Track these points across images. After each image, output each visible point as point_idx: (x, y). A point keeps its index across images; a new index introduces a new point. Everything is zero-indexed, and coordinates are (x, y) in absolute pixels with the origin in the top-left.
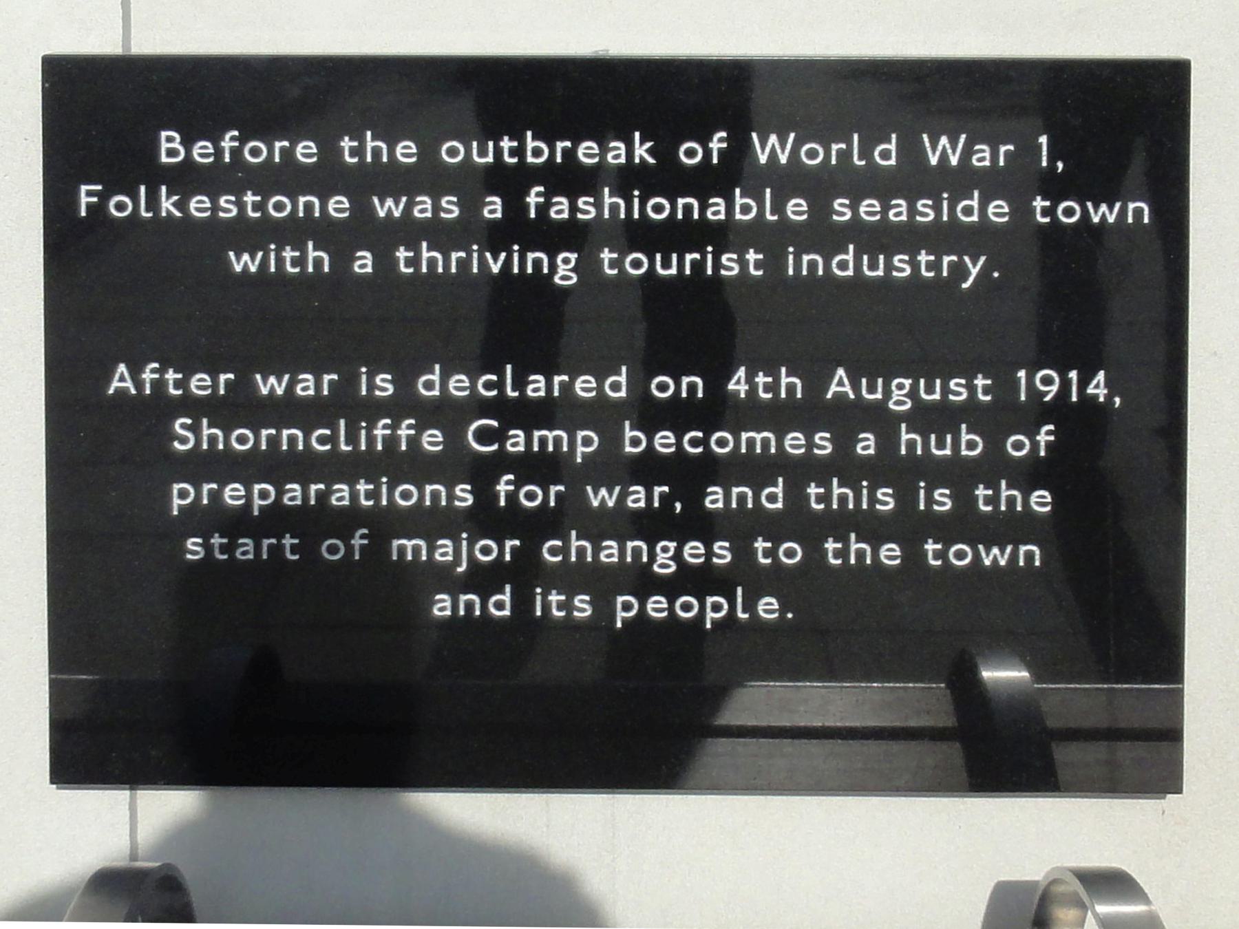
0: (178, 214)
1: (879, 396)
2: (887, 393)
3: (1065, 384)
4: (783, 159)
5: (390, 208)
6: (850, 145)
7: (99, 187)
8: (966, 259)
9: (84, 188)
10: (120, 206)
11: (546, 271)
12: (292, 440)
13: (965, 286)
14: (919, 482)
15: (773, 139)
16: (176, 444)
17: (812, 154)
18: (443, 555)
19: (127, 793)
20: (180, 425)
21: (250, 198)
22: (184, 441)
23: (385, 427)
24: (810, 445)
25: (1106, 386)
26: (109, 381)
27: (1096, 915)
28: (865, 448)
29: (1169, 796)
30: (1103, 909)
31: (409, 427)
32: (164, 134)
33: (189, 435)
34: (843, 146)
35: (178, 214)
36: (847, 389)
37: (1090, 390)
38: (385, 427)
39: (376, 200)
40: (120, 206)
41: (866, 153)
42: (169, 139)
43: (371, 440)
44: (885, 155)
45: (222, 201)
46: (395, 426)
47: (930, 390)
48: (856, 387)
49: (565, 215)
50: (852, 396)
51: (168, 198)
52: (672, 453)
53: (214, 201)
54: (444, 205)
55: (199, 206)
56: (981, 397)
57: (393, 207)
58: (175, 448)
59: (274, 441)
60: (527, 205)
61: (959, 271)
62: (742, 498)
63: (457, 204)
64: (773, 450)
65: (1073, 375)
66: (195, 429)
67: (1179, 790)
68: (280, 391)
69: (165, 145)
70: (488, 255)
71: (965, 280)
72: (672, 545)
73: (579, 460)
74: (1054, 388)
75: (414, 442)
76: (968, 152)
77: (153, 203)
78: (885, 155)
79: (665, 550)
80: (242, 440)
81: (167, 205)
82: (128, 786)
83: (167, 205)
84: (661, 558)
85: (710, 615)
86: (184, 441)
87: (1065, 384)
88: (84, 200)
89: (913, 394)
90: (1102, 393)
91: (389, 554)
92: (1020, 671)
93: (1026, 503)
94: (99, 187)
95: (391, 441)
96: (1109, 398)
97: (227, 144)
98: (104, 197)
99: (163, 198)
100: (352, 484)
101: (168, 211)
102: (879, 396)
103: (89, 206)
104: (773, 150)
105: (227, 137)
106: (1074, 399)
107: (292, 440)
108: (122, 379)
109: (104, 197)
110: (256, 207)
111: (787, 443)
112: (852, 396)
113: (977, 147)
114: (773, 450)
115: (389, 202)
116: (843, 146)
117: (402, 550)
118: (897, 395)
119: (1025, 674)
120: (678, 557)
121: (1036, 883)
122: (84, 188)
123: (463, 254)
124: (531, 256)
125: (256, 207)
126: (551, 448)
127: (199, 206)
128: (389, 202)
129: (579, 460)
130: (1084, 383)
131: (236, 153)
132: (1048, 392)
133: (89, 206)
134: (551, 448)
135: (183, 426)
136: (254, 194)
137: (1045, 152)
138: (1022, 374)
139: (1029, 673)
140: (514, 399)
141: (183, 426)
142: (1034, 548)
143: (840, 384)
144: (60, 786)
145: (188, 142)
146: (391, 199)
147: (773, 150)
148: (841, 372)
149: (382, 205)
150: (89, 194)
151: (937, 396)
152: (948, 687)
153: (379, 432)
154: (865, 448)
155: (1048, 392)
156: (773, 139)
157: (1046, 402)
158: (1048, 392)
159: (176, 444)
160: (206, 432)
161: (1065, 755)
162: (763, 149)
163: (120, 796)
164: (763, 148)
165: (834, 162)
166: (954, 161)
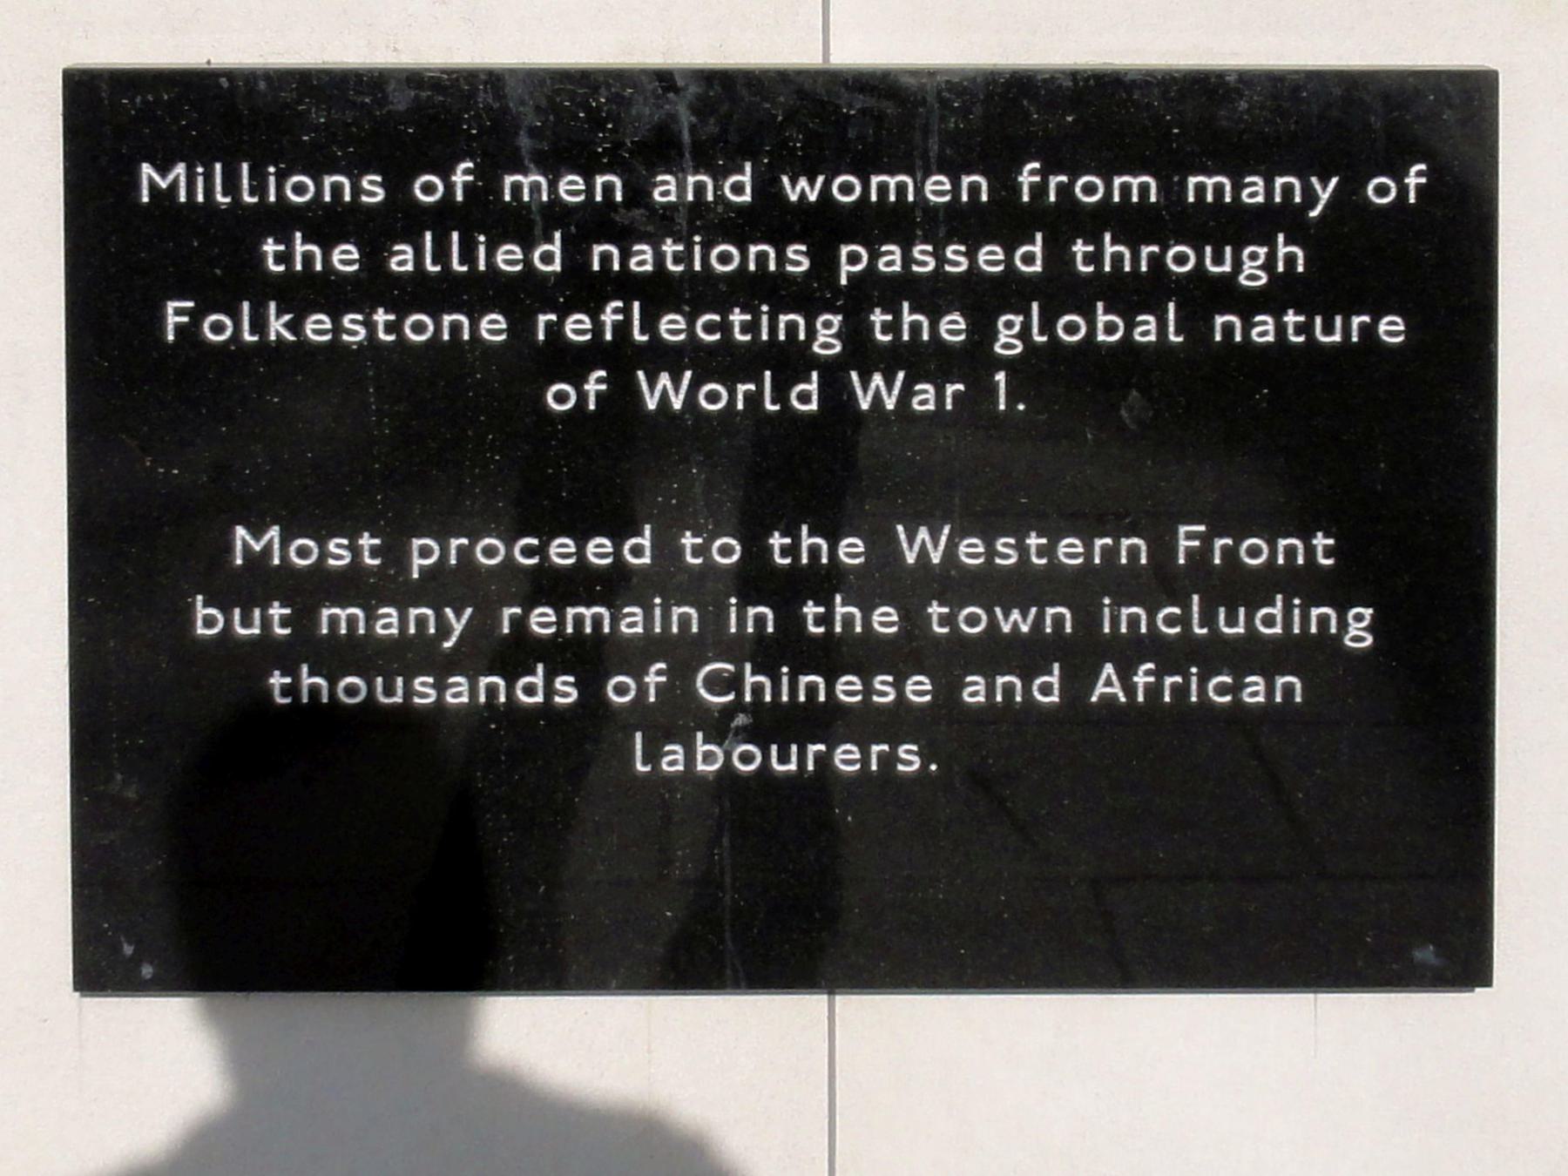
0: (290, 337)
2: (1238, 265)
7: (190, 304)
10: (217, 329)
11: (802, 336)
14: (1189, 667)
19: (825, 997)
21: (381, 317)
24: (868, 690)
28: (672, 763)
29: (1478, 990)
34: (752, 387)
35: (290, 337)
39: (785, 180)
40: (217, 329)
41: (780, 395)
44: (804, 398)
49: (897, 268)
51: (278, 317)
52: (730, 702)
53: (336, 321)
54: (1000, 548)
55: (317, 326)
57: (807, 189)
62: (1009, 690)
67: (1486, 981)
77: (259, 325)
81: (277, 327)
82: (826, 991)
83: (277, 327)
84: (1249, 267)
88: (172, 320)
91: (1212, 329)
93: (919, 190)
94: (190, 304)
98: (197, 316)
99: (272, 318)
101: (278, 334)
102: (1227, 268)
105: (608, 310)
110: (389, 328)
111: (840, 688)
116: (752, 387)
117: (334, 621)
125: (389, 328)
126: (1210, 198)
127: (317, 326)
134: (1210, 198)
136: (386, 312)
140: (783, 567)
144: (84, 993)
146: (805, 178)
150: (178, 312)
151: (398, 699)
154: (672, 763)
156: (878, 380)
163: (811, 1005)
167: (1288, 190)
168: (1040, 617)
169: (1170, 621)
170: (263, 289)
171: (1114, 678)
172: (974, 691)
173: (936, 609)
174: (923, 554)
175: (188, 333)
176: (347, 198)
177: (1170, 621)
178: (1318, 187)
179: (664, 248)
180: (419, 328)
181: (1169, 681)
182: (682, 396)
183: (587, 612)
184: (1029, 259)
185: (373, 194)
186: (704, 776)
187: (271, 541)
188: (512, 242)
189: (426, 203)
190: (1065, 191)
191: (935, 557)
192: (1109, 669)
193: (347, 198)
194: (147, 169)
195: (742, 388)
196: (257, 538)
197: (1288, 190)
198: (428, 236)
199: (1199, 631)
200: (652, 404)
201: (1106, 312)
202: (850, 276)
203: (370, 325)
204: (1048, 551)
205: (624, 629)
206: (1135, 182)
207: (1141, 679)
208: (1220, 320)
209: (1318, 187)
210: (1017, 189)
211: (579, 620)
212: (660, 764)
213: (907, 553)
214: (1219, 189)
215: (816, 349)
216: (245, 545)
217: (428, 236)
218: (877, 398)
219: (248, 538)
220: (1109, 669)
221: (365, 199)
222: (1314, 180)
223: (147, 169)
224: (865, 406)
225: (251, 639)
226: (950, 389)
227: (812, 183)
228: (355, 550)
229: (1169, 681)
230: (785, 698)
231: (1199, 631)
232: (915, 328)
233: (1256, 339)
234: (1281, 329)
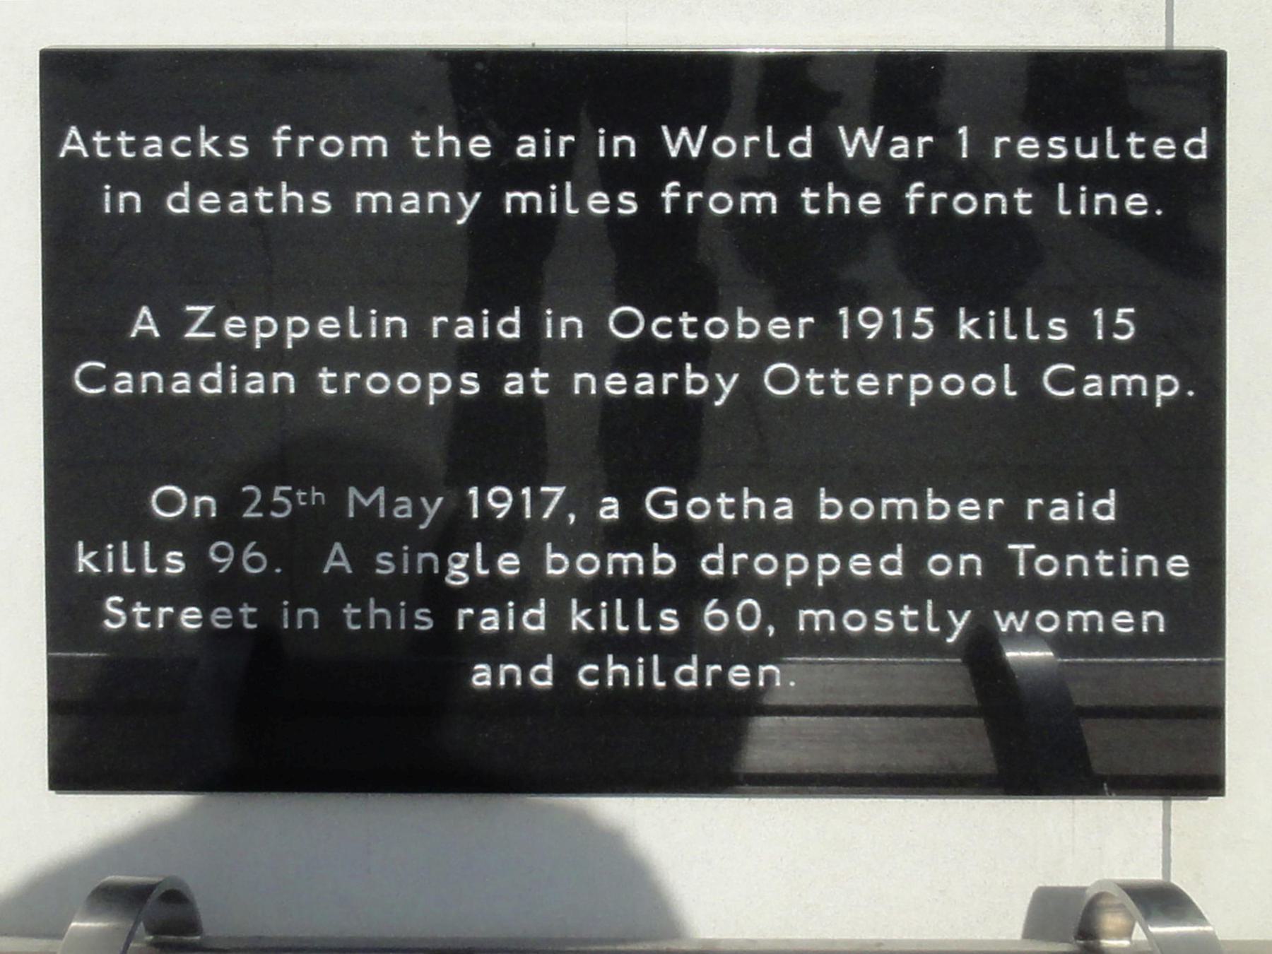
3: (890, 321)
4: (695, 153)
5: (1012, 623)
6: (764, 139)
11: (436, 571)
15: (861, 133)
17: (724, 147)
18: (180, 387)
20: (112, 603)
22: (115, 619)
26: (129, 327)
33: (120, 612)
36: (81, 147)
41: (780, 145)
44: (800, 147)
50: (85, 155)
58: (106, 626)
60: (274, 144)
63: (329, 199)
64: (1101, 629)
66: (126, 606)
71: (718, 398)
73: (432, 403)
76: (886, 144)
78: (800, 147)
85: (291, 336)
86: (115, 619)
92: (1042, 650)
100: (250, 191)
104: (684, 144)
108: (145, 322)
112: (85, 155)
113: (895, 139)
114: (1101, 629)
115: (1012, 617)
116: (757, 139)
119: (1051, 654)
124: (564, 321)
128: (1012, 617)
129: (432, 403)
132: (871, 330)
135: (115, 605)
137: (965, 144)
139: (1053, 652)
141: (115, 605)
142: (574, 319)
147: (684, 144)
149: (1004, 620)
152: (964, 662)
155: (872, 330)
156: (861, 133)
157: (869, 339)
158: (871, 330)
159: (108, 624)
162: (674, 141)
164: (674, 141)
165: (747, 155)
166: (871, 152)
167: (439, 203)
171: (78, 138)
172: (785, 509)
174: (684, 149)
176: (301, 210)
178: (464, 200)
179: (1097, 558)
181: (302, 139)
182: (699, 145)
185: (321, 207)
187: (378, 498)
189: (596, 214)
190: (945, 205)
191: (871, 151)
192: (73, 131)
193: (301, 210)
194: (353, 492)
195: (748, 140)
196: (367, 496)
197: (439, 203)
199: (149, 570)
200: (850, 153)
201: (935, 496)
202: (826, 580)
204: (849, 384)
206: (523, 197)
208: (578, 377)
209: (464, 200)
210: (662, 202)
212: (142, 151)
213: (847, 149)
214: (531, 202)
216: (356, 501)
219: (359, 496)
220: (73, 131)
221: (315, 211)
222: (424, 500)
223: (353, 492)
224: (674, 154)
226: (802, 321)
229: (302, 139)
230: (548, 154)
231: (149, 570)
232: (839, 204)
233: (778, 517)
234: (528, 384)
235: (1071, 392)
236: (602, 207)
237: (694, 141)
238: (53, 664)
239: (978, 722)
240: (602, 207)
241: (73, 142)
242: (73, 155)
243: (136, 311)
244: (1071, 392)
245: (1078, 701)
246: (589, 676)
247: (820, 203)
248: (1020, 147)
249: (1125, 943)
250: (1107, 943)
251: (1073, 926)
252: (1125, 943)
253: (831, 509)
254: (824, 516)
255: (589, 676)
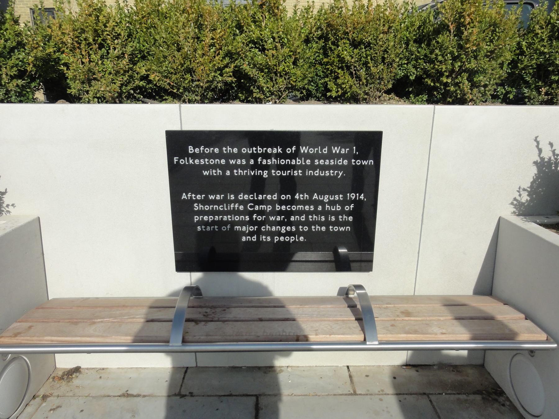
1: (322, 199)
3: (356, 196)
7: (178, 158)
8: (339, 172)
9: (175, 158)
10: (182, 162)
12: (216, 208)
13: (339, 177)
16: (195, 209)
20: (195, 205)
21: (206, 160)
22: (196, 208)
23: (233, 205)
25: (364, 197)
27: (356, 292)
30: (357, 292)
31: (237, 205)
32: (190, 147)
33: (197, 207)
36: (317, 197)
37: (360, 197)
38: (233, 205)
40: (182, 162)
41: (321, 151)
42: (191, 148)
43: (230, 208)
45: (201, 160)
46: (235, 205)
47: (332, 197)
48: (318, 197)
51: (280, 148)
56: (341, 199)
59: (213, 208)
61: (338, 174)
65: (358, 194)
66: (198, 206)
68: (213, 198)
69: (190, 149)
70: (251, 171)
71: (339, 176)
72: (285, 227)
74: (354, 197)
75: (238, 208)
77: (188, 161)
79: (283, 228)
80: (207, 208)
81: (191, 161)
83: (191, 161)
84: (283, 230)
86: (196, 208)
87: (356, 196)
88: (175, 160)
89: (329, 198)
90: (363, 198)
91: (234, 229)
94: (178, 158)
95: (234, 208)
96: (364, 199)
97: (202, 149)
98: (179, 160)
102: (322, 199)
103: (176, 162)
105: (202, 147)
106: (358, 199)
107: (216, 208)
109: (179, 160)
115: (212, 196)
117: (236, 228)
118: (326, 198)
119: (346, 250)
120: (286, 229)
121: (346, 287)
122: (175, 158)
123: (246, 171)
125: (208, 162)
127: (197, 161)
128: (212, 196)
130: (359, 196)
131: (203, 151)
133: (176, 162)
135: (196, 205)
138: (348, 194)
141: (196, 205)
143: (315, 197)
145: (194, 149)
148: (316, 194)
150: (176, 159)
153: (232, 206)
159: (195, 209)
160: (200, 206)
161: (353, 265)
168: (346, 228)
169: (221, 208)
170: (189, 156)
173: (300, 227)
175: (178, 162)
177: (221, 208)
180: (212, 162)
183: (263, 206)
184: (275, 197)
186: (259, 153)
188: (246, 194)
192: (184, 194)
198: (186, 158)
199: (225, 209)
203: (205, 161)
205: (238, 163)
207: (189, 195)
211: (262, 208)
215: (282, 232)
217: (186, 158)
218: (304, 151)
220: (184, 194)
225: (334, 211)
226: (203, 196)
227: (343, 228)
228: (339, 197)
231: (225, 209)
235: (253, 209)
236: (198, 151)
237: (306, 150)
238: (175, 254)
239: (413, 294)
240: (198, 151)
241: (184, 196)
242: (184, 199)
243: (182, 195)
244: (253, 209)
245: (350, 259)
246: (264, 229)
247: (312, 218)
248: (268, 150)
249: (353, 296)
250: (350, 296)
251: (345, 293)
252: (353, 296)
253: (278, 208)
254: (277, 209)
255: (264, 229)
